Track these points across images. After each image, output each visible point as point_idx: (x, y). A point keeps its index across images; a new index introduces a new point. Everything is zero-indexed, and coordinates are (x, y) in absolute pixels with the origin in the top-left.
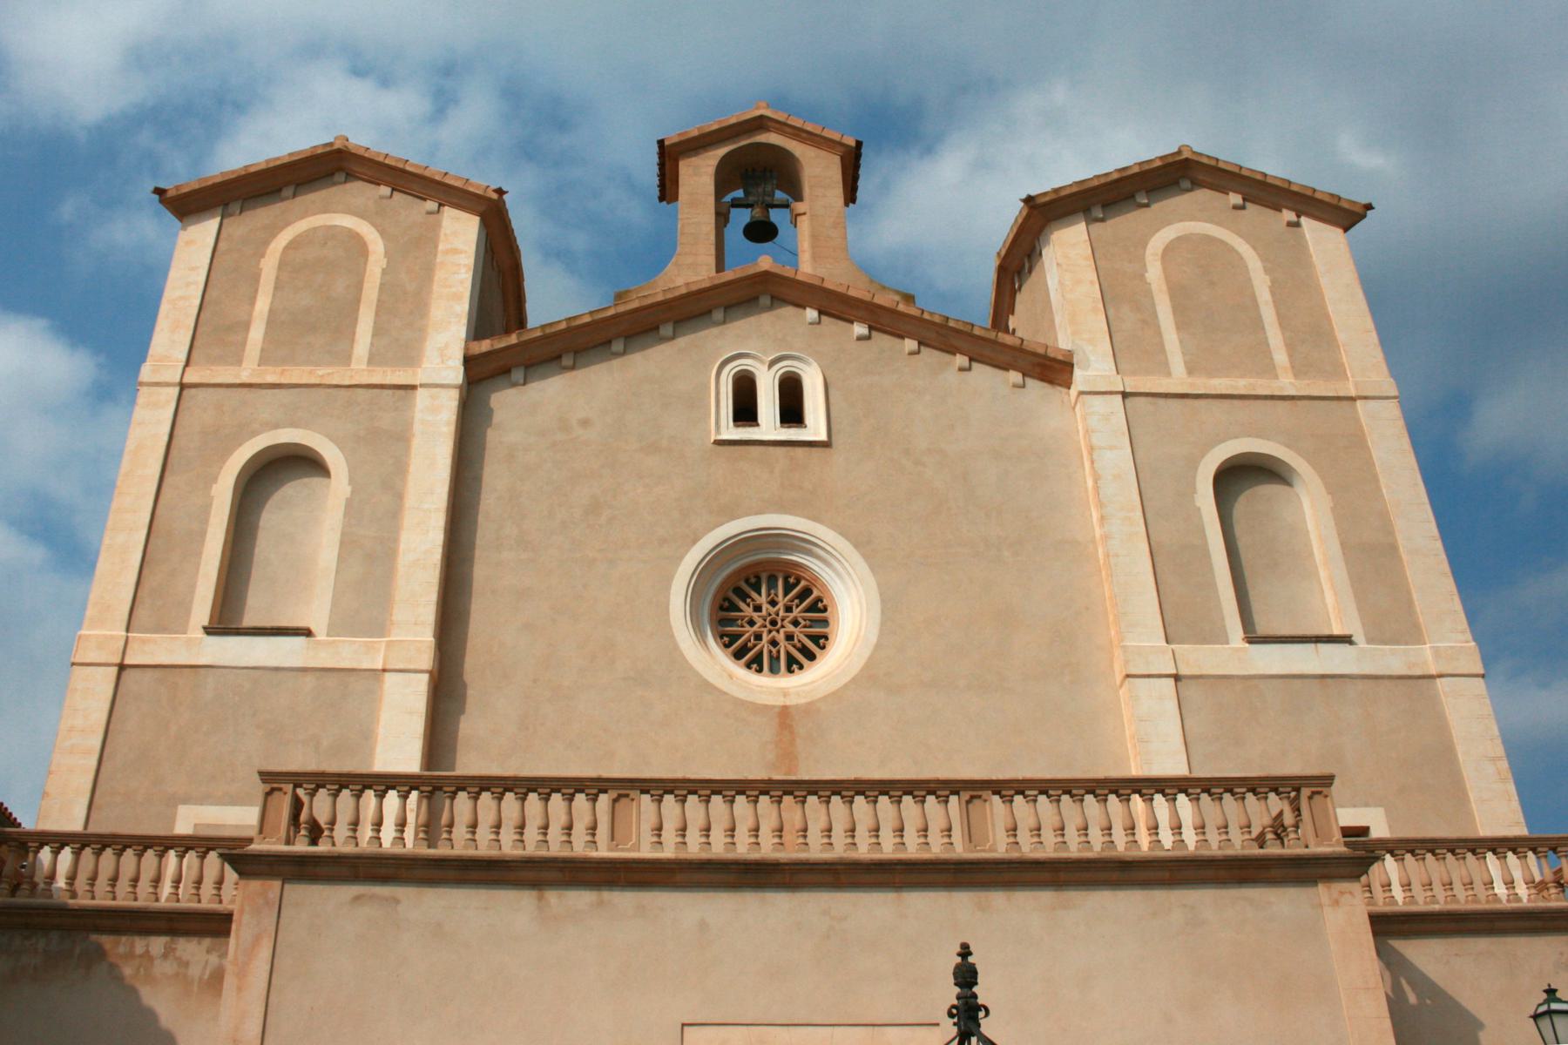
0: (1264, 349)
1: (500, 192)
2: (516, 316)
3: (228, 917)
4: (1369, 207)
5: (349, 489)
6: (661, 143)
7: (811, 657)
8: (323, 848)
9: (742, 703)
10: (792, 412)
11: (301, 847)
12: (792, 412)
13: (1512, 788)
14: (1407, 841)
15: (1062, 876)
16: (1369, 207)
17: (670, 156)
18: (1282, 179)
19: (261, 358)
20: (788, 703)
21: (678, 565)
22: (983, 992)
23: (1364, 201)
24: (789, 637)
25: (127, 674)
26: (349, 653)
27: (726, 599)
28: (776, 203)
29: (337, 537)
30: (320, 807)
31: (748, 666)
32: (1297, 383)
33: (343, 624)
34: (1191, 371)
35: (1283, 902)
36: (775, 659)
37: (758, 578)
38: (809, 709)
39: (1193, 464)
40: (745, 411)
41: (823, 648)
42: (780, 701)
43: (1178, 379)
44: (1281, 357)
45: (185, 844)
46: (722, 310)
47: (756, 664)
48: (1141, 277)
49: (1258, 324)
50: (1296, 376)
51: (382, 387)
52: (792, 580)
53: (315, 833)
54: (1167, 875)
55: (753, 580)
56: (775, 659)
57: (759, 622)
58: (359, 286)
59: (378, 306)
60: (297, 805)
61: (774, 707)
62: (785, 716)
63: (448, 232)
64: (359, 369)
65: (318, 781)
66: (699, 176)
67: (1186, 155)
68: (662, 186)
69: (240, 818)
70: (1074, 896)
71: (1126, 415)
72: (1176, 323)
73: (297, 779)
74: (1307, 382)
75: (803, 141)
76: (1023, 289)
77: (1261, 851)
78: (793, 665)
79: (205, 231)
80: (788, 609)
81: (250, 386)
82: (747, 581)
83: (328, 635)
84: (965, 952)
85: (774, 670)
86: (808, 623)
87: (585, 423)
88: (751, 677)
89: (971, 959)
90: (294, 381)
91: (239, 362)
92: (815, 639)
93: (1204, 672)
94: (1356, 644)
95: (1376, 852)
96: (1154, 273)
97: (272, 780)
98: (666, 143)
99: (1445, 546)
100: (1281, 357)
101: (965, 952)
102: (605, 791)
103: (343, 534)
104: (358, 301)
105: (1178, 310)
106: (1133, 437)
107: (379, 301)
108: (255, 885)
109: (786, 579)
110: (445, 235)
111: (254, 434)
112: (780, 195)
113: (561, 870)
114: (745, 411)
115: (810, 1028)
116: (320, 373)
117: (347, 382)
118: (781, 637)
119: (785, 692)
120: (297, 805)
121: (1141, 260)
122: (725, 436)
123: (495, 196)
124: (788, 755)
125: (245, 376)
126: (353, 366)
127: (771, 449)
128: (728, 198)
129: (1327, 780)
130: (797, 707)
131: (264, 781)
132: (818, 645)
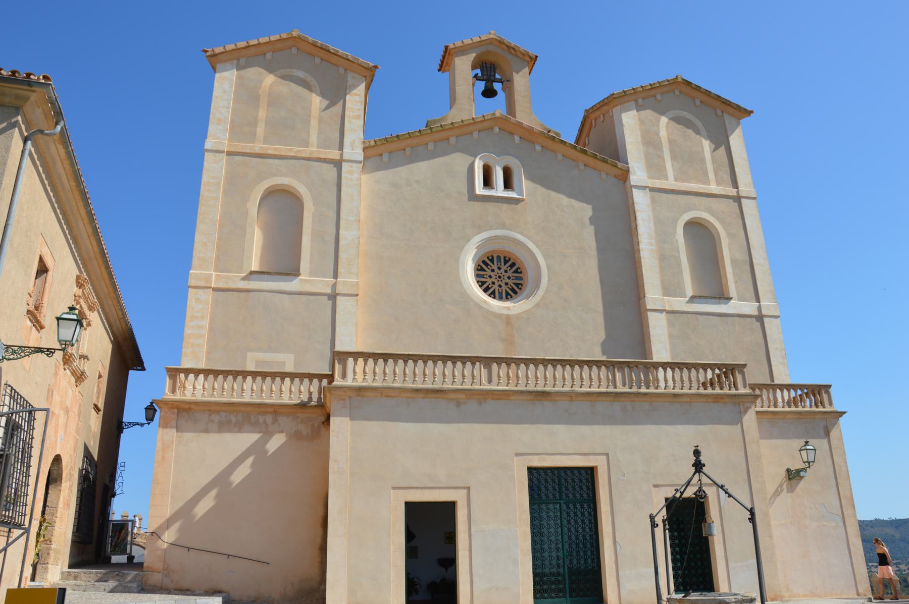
0: (705, 172)
12: (508, 185)
14: (758, 385)
18: (717, 95)
19: (264, 141)
20: (510, 314)
22: (703, 458)
24: (506, 284)
31: (490, 295)
34: (676, 180)
36: (500, 294)
39: (675, 221)
40: (488, 182)
41: (520, 289)
42: (505, 312)
43: (671, 183)
44: (711, 176)
46: (477, 132)
50: (717, 185)
61: (505, 315)
71: (107, 267)
72: (671, 157)
80: (506, 271)
82: (505, 257)
86: (485, 276)
92: (517, 285)
95: (808, 399)
100: (711, 176)
105: (672, 152)
110: (349, 85)
114: (488, 182)
115: (15, 207)
130: (513, 315)
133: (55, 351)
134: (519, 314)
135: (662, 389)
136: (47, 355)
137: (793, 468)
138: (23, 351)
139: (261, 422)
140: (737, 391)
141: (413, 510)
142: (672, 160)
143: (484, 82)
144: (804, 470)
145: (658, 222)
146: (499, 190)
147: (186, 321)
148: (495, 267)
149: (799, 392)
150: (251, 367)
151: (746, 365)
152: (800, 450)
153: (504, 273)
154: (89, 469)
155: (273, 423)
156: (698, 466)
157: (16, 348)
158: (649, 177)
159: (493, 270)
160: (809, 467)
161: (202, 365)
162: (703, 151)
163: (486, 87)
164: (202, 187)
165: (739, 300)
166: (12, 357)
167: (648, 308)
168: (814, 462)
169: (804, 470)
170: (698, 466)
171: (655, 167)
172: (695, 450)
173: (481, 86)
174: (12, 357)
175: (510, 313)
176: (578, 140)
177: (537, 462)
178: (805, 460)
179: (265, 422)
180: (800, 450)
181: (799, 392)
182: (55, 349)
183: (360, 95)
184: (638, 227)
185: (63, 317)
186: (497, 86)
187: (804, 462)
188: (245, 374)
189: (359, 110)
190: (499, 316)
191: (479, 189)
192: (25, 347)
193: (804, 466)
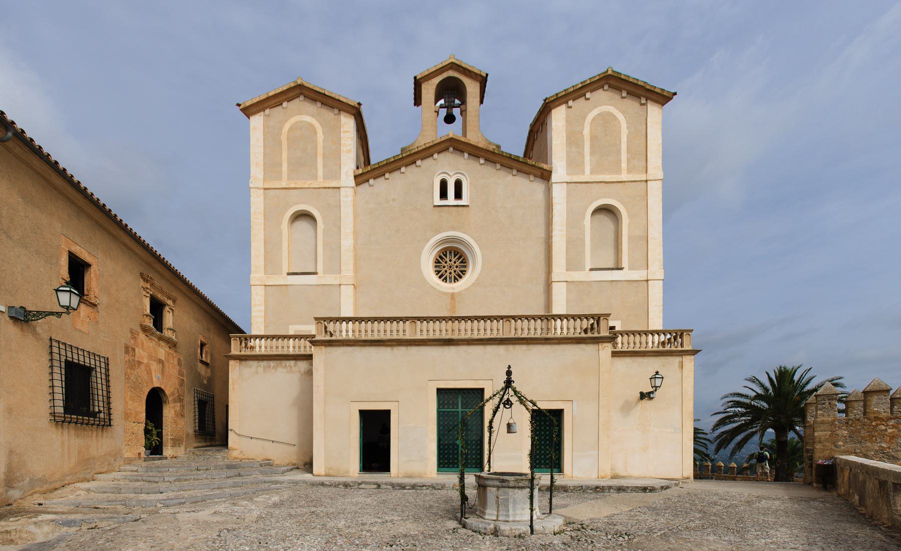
0: (619, 162)
1: (359, 104)
2: (367, 161)
3: (311, 355)
4: (675, 94)
5: (323, 226)
6: (415, 78)
7: (461, 277)
8: (334, 338)
9: (439, 291)
10: (458, 195)
11: (328, 338)
12: (458, 195)
13: (662, 315)
15: (529, 342)
16: (675, 94)
17: (418, 84)
19: (288, 178)
21: (423, 249)
22: (513, 377)
23: (673, 91)
25: (645, 183)
26: (330, 280)
27: (437, 259)
28: (455, 106)
29: (322, 243)
30: (331, 327)
32: (628, 176)
33: (327, 271)
35: (590, 349)
36: (450, 278)
37: (446, 253)
38: (460, 293)
39: (586, 209)
40: (458, 185)
42: (451, 291)
45: (295, 337)
47: (445, 280)
48: (581, 133)
49: (619, 152)
51: (329, 188)
52: (456, 253)
53: (331, 335)
54: (557, 341)
55: (445, 253)
56: (450, 278)
57: (454, 267)
58: (316, 147)
59: (323, 156)
60: (326, 327)
61: (450, 293)
62: (453, 296)
63: (343, 123)
64: (320, 182)
65: (331, 320)
66: (429, 90)
67: (610, 72)
68: (415, 99)
69: (311, 329)
70: (531, 346)
73: (325, 319)
74: (631, 175)
75: (466, 75)
76: (605, 92)
77: (598, 335)
78: (456, 280)
79: (257, 121)
80: (455, 262)
81: (286, 188)
83: (323, 274)
84: (509, 367)
85: (451, 282)
87: (394, 200)
88: (443, 284)
89: (510, 369)
90: (300, 186)
91: (281, 179)
92: (439, 262)
93: (574, 280)
94: (69, 251)
96: (587, 131)
97: (318, 319)
98: (418, 78)
99: (663, 236)
101: (509, 367)
102: (408, 320)
103: (323, 241)
104: (316, 153)
105: (592, 146)
106: (282, 286)
107: (323, 153)
108: (318, 348)
109: (454, 252)
111: (291, 206)
112: (457, 102)
113: (396, 342)
114: (444, 195)
116: (308, 183)
117: (317, 187)
118: (448, 272)
119: (453, 288)
120: (326, 327)
121: (583, 125)
122: (436, 204)
123: (357, 106)
124: (453, 308)
125: (284, 185)
126: (318, 180)
127: (451, 208)
128: (438, 104)
129: (609, 315)
131: (315, 320)
132: (463, 274)
133: (62, 314)
134: (460, 292)
135: (531, 335)
136: (57, 317)
137: (645, 391)
138: (41, 315)
139: (288, 365)
140: (598, 335)
141: (365, 415)
142: (590, 155)
143: (446, 109)
144: (652, 392)
145: (570, 211)
146: (451, 199)
147: (252, 308)
148: (457, 263)
149: (668, 336)
150: (291, 333)
151: (610, 314)
152: (651, 379)
153: (453, 264)
154: (788, 431)
155: (295, 366)
156: (509, 383)
157: (35, 313)
158: (568, 174)
159: (455, 262)
160: (656, 390)
161: (262, 333)
162: (620, 143)
163: (447, 113)
164: (252, 216)
165: (629, 269)
166: (33, 319)
167: (553, 280)
168: (660, 387)
169: (652, 392)
170: (509, 383)
171: (574, 164)
172: (507, 371)
173: (443, 112)
174: (33, 319)
175: (454, 291)
176: (526, 154)
177: (443, 385)
178: (653, 385)
179: (290, 366)
180: (57, 290)
181: (668, 336)
182: (62, 313)
183: (350, 132)
184: (554, 217)
185: (61, 289)
186: (456, 112)
187: (652, 387)
188: (289, 337)
189: (350, 145)
190: (446, 294)
191: (437, 201)
192: (41, 312)
193: (651, 390)
